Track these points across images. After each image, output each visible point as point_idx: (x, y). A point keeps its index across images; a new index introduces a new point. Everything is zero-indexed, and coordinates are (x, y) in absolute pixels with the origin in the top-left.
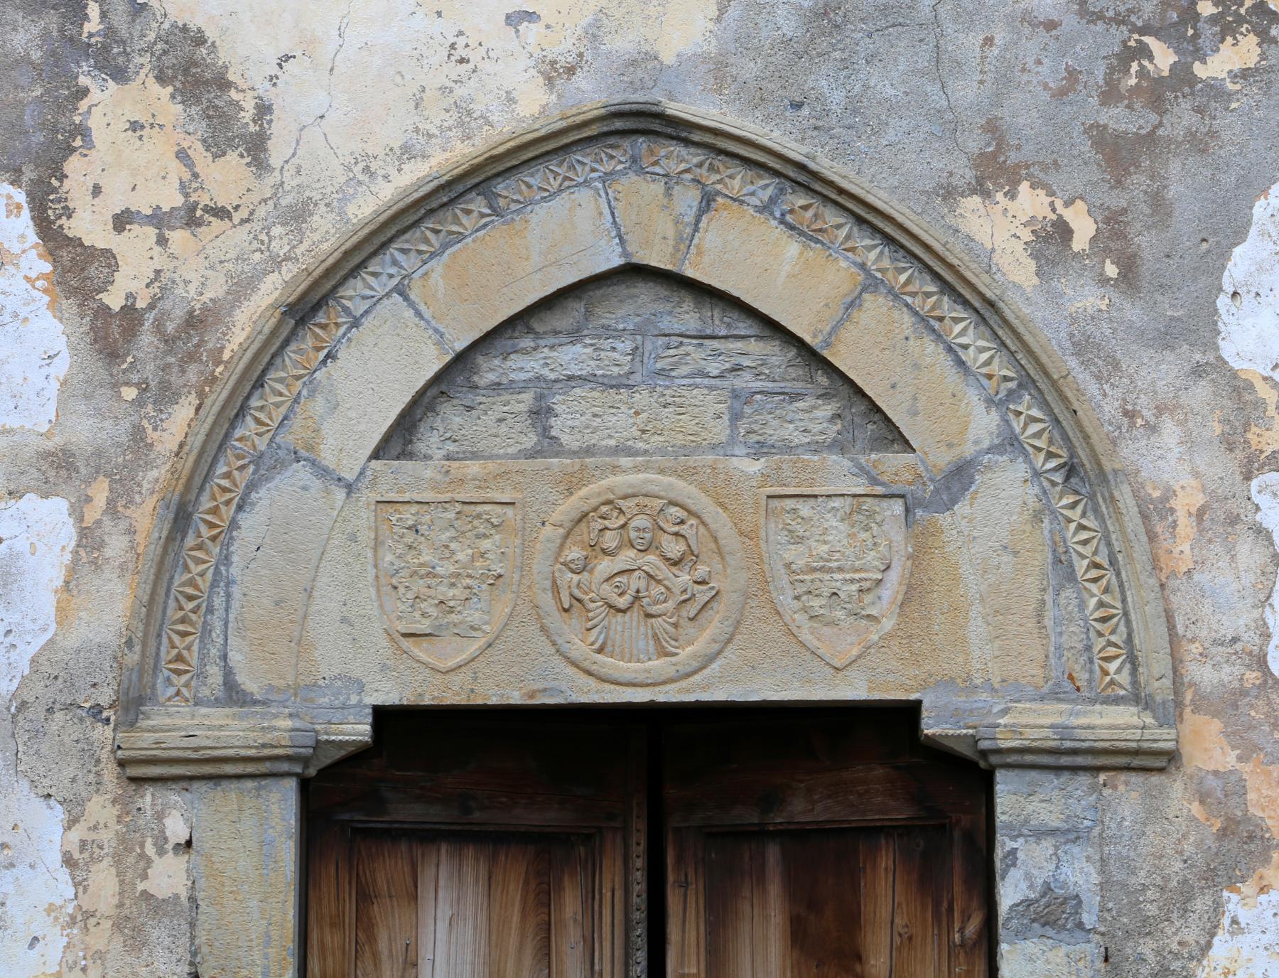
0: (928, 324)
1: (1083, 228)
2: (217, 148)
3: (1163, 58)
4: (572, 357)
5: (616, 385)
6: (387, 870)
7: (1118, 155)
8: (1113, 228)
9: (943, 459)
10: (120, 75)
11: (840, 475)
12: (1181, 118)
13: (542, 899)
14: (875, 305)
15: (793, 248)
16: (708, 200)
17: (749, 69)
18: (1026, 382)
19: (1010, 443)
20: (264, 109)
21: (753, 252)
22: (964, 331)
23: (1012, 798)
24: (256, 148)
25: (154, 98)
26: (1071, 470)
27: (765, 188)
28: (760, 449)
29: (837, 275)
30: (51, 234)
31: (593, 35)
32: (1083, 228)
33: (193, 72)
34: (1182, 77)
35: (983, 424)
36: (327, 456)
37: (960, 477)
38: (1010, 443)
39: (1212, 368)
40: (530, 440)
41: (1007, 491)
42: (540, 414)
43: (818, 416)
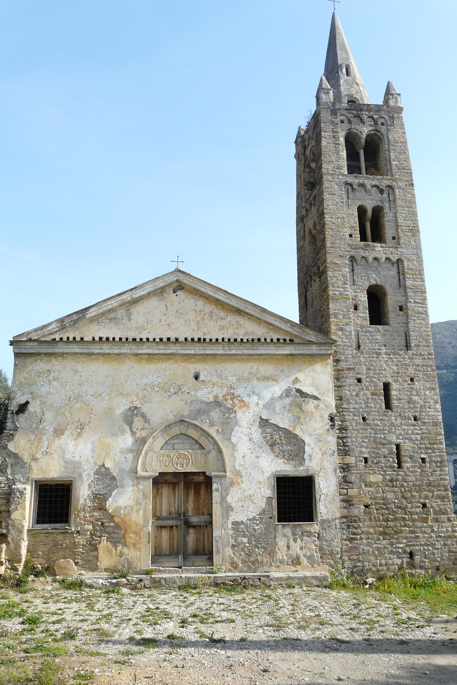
0: (207, 438)
1: (220, 430)
2: (145, 423)
3: (227, 415)
4: (176, 441)
5: (180, 443)
6: (160, 486)
7: (223, 423)
8: (222, 429)
9: (208, 450)
10: (137, 417)
11: (199, 452)
12: (229, 420)
13: (174, 488)
14: (202, 436)
15: (195, 432)
16: (188, 427)
17: (192, 416)
18: (215, 443)
19: (214, 449)
20: (150, 419)
22: (210, 439)
23: (213, 480)
24: (149, 423)
25: (140, 418)
26: (219, 451)
27: (193, 426)
28: (192, 449)
29: (199, 434)
30: (131, 431)
31: (178, 413)
32: (220, 430)
33: (144, 416)
34: (229, 417)
35: (211, 447)
36: (155, 450)
37: (209, 452)
38: (214, 449)
39: (231, 442)
40: (172, 448)
41: (214, 453)
42: (173, 446)
43: (197, 446)
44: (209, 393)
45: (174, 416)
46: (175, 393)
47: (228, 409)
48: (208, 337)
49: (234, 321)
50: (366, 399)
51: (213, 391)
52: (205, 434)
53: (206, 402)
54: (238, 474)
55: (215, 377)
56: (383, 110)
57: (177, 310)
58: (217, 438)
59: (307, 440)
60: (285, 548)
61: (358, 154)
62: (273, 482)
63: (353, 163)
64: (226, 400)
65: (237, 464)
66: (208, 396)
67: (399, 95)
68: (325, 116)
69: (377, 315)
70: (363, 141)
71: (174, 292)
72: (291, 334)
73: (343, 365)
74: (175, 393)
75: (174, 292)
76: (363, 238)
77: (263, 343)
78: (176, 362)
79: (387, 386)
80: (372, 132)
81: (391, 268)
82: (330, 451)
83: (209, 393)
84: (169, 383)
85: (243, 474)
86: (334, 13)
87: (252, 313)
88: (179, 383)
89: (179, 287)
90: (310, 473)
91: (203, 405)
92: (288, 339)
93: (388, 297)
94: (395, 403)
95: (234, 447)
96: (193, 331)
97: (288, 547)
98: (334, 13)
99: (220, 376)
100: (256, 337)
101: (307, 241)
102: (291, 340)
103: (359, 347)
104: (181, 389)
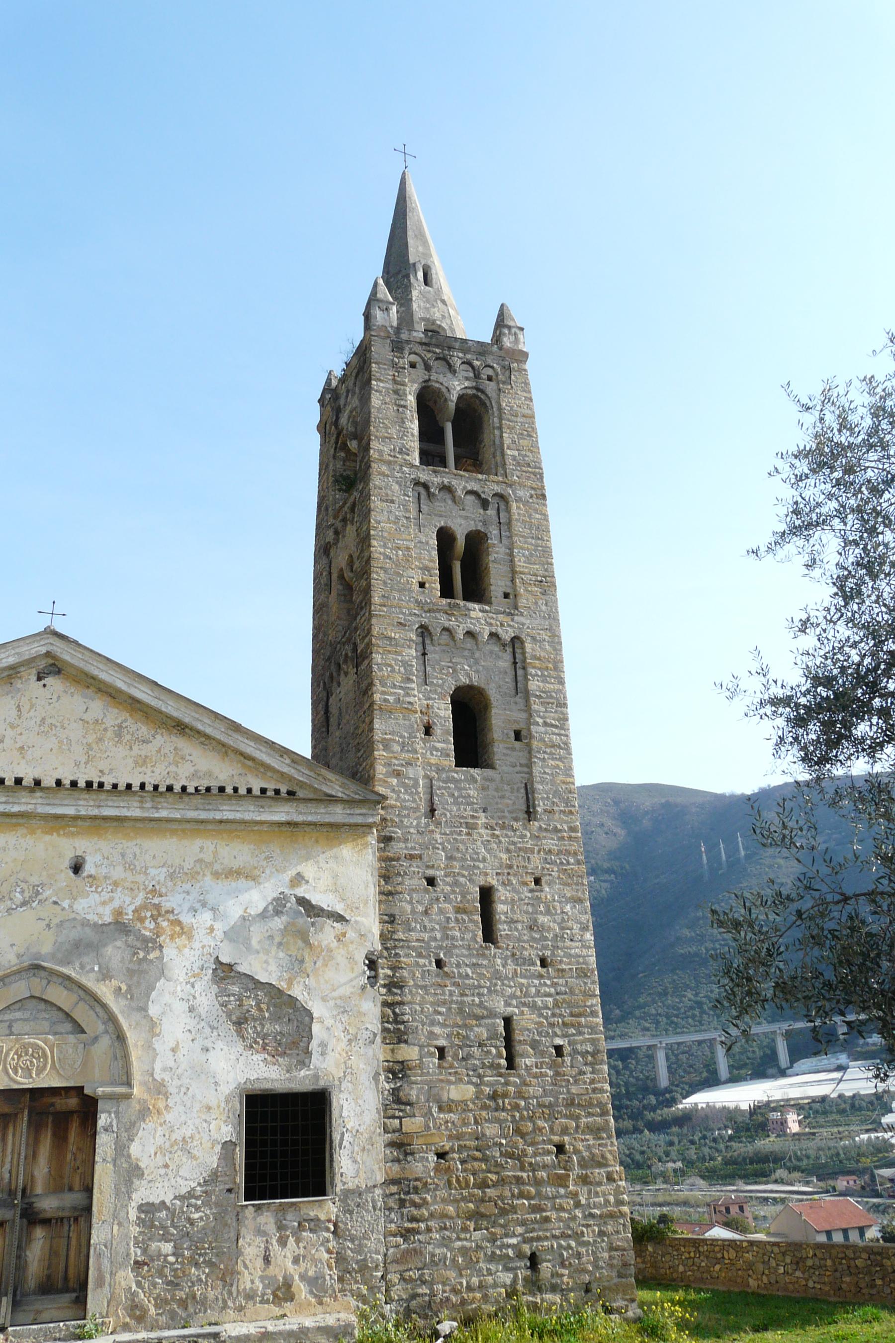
8: (129, 987)
11: (72, 1038)
21: (58, 995)
22: (99, 1009)
23: (101, 1105)
29: (74, 998)
35: (101, 1028)
37: (96, 1039)
41: (105, 1042)
43: (68, 1026)
44: (104, 903)
45: (19, 956)
46: (24, 904)
47: (145, 940)
48: (108, 781)
49: (168, 748)
50: (441, 920)
51: (111, 899)
52: (87, 998)
53: (95, 925)
54: (159, 1089)
55: (120, 869)
56: (492, 353)
57: (43, 719)
58: (116, 1006)
59: (317, 1009)
60: (260, 1262)
61: (441, 432)
62: (239, 1107)
63: (432, 447)
64: (142, 920)
65: (158, 1066)
66: (100, 910)
67: (522, 329)
68: (381, 351)
69: (471, 746)
70: (452, 406)
71: (39, 679)
72: (291, 779)
73: (398, 848)
74: (24, 904)
75: (39, 679)
76: (447, 591)
77: (230, 797)
78: (32, 832)
79: (486, 894)
80: (470, 392)
81: (501, 654)
82: (367, 1035)
83: (104, 903)
84: (12, 880)
85: (172, 1090)
86: (404, 173)
87: (208, 731)
88: (35, 880)
89: (52, 667)
90: (322, 1084)
91: (88, 930)
92: (284, 790)
93: (494, 711)
94: (502, 929)
95: (153, 1027)
96: (77, 764)
97: (267, 1260)
98: (404, 173)
99: (130, 867)
100: (215, 784)
101: (334, 593)
102: (291, 793)
103: (433, 810)
104: (38, 893)
